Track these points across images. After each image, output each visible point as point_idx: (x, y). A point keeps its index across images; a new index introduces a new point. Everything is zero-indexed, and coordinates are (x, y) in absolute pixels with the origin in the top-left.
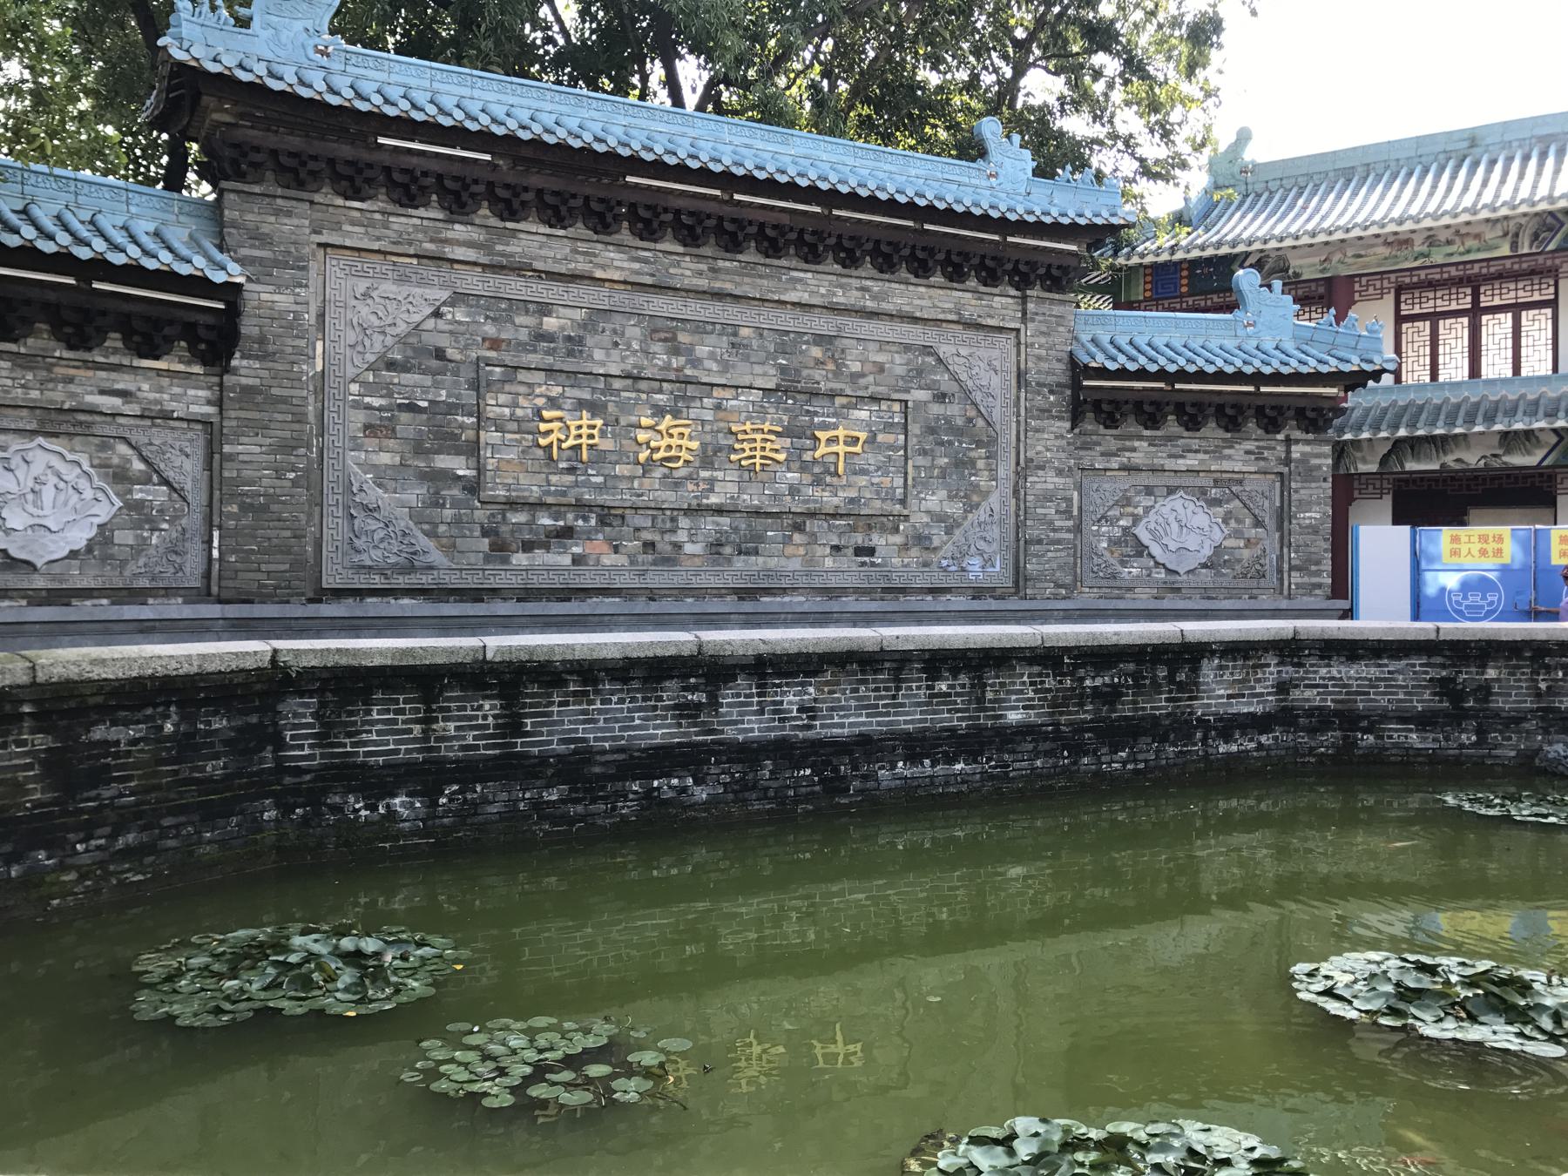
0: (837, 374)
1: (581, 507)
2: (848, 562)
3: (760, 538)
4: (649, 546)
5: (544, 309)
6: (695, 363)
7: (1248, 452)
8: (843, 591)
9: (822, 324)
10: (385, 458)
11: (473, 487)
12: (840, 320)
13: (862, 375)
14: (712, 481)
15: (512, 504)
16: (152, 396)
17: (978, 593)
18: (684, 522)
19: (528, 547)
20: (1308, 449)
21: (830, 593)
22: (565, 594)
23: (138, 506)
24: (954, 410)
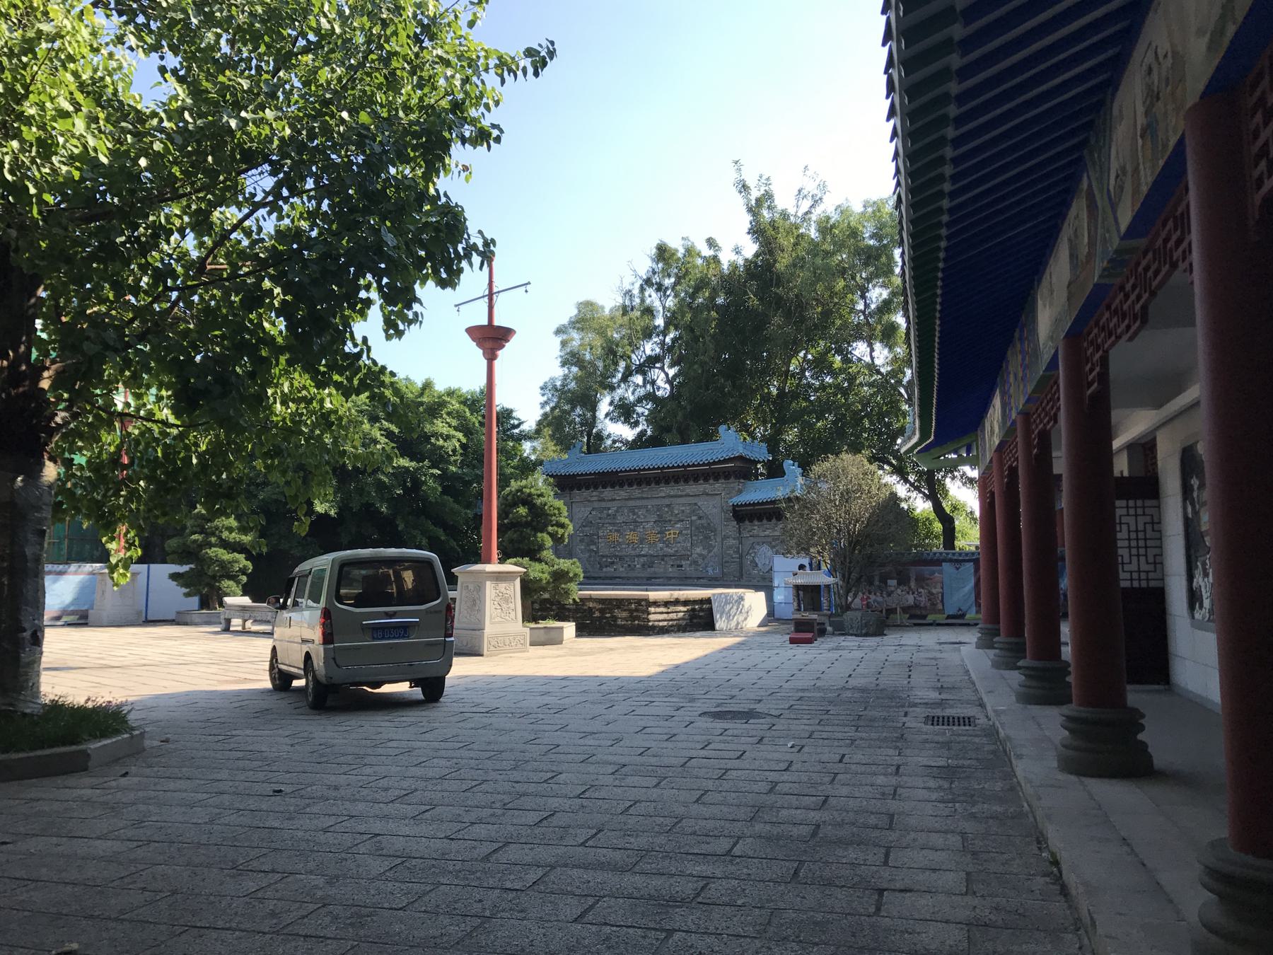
1: (616, 556)
2: (675, 569)
9: (667, 501)
11: (596, 552)
17: (711, 579)
21: (670, 578)
22: (611, 578)
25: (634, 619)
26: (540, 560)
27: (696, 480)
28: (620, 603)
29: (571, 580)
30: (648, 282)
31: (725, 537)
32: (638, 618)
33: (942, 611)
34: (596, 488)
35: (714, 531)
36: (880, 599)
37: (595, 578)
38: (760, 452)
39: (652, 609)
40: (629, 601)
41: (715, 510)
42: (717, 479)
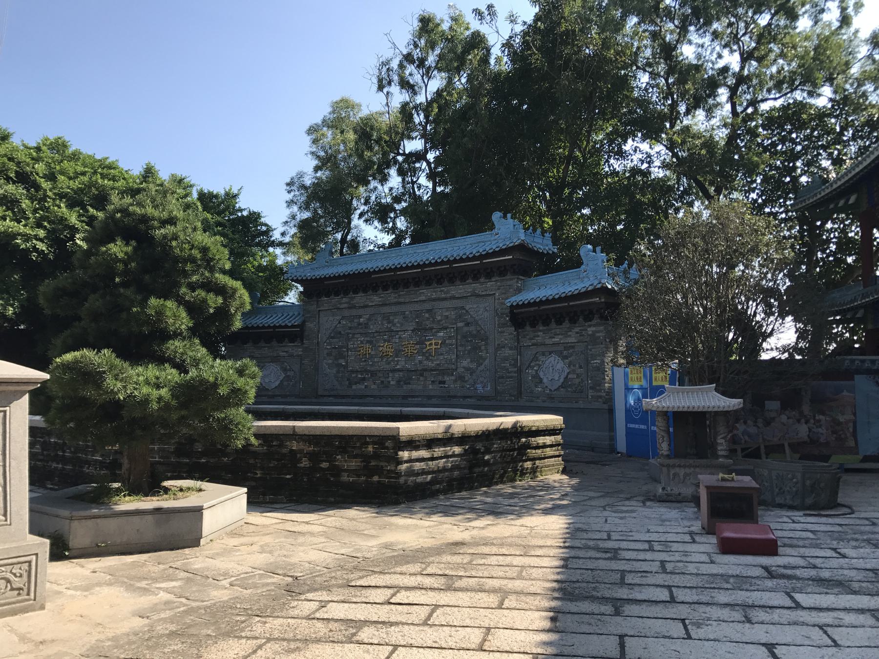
0: (433, 322)
1: (367, 371)
3: (411, 379)
4: (382, 382)
5: (360, 317)
6: (394, 325)
7: (577, 333)
8: (434, 397)
9: (427, 306)
10: (330, 361)
11: (346, 367)
12: (433, 303)
13: (441, 320)
14: (398, 361)
15: (352, 372)
16: (466, 329)
17: (481, 398)
18: (391, 375)
19: (356, 383)
20: (594, 329)
21: (430, 397)
22: (361, 397)
23: (288, 376)
24: (472, 328)
25: (370, 471)
26: (161, 360)
27: (463, 279)
28: (345, 441)
29: (225, 402)
30: (408, 58)
31: (500, 347)
32: (379, 471)
33: (854, 451)
34: (346, 293)
35: (485, 339)
36: (753, 430)
37: (343, 397)
38: (544, 244)
39: (405, 455)
40: (362, 438)
41: (486, 314)
42: (489, 276)
